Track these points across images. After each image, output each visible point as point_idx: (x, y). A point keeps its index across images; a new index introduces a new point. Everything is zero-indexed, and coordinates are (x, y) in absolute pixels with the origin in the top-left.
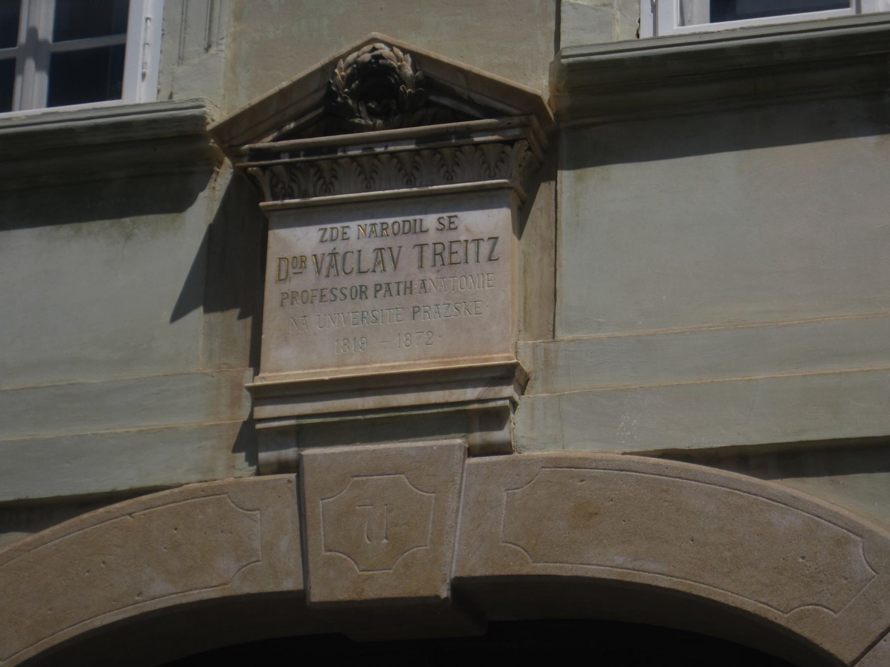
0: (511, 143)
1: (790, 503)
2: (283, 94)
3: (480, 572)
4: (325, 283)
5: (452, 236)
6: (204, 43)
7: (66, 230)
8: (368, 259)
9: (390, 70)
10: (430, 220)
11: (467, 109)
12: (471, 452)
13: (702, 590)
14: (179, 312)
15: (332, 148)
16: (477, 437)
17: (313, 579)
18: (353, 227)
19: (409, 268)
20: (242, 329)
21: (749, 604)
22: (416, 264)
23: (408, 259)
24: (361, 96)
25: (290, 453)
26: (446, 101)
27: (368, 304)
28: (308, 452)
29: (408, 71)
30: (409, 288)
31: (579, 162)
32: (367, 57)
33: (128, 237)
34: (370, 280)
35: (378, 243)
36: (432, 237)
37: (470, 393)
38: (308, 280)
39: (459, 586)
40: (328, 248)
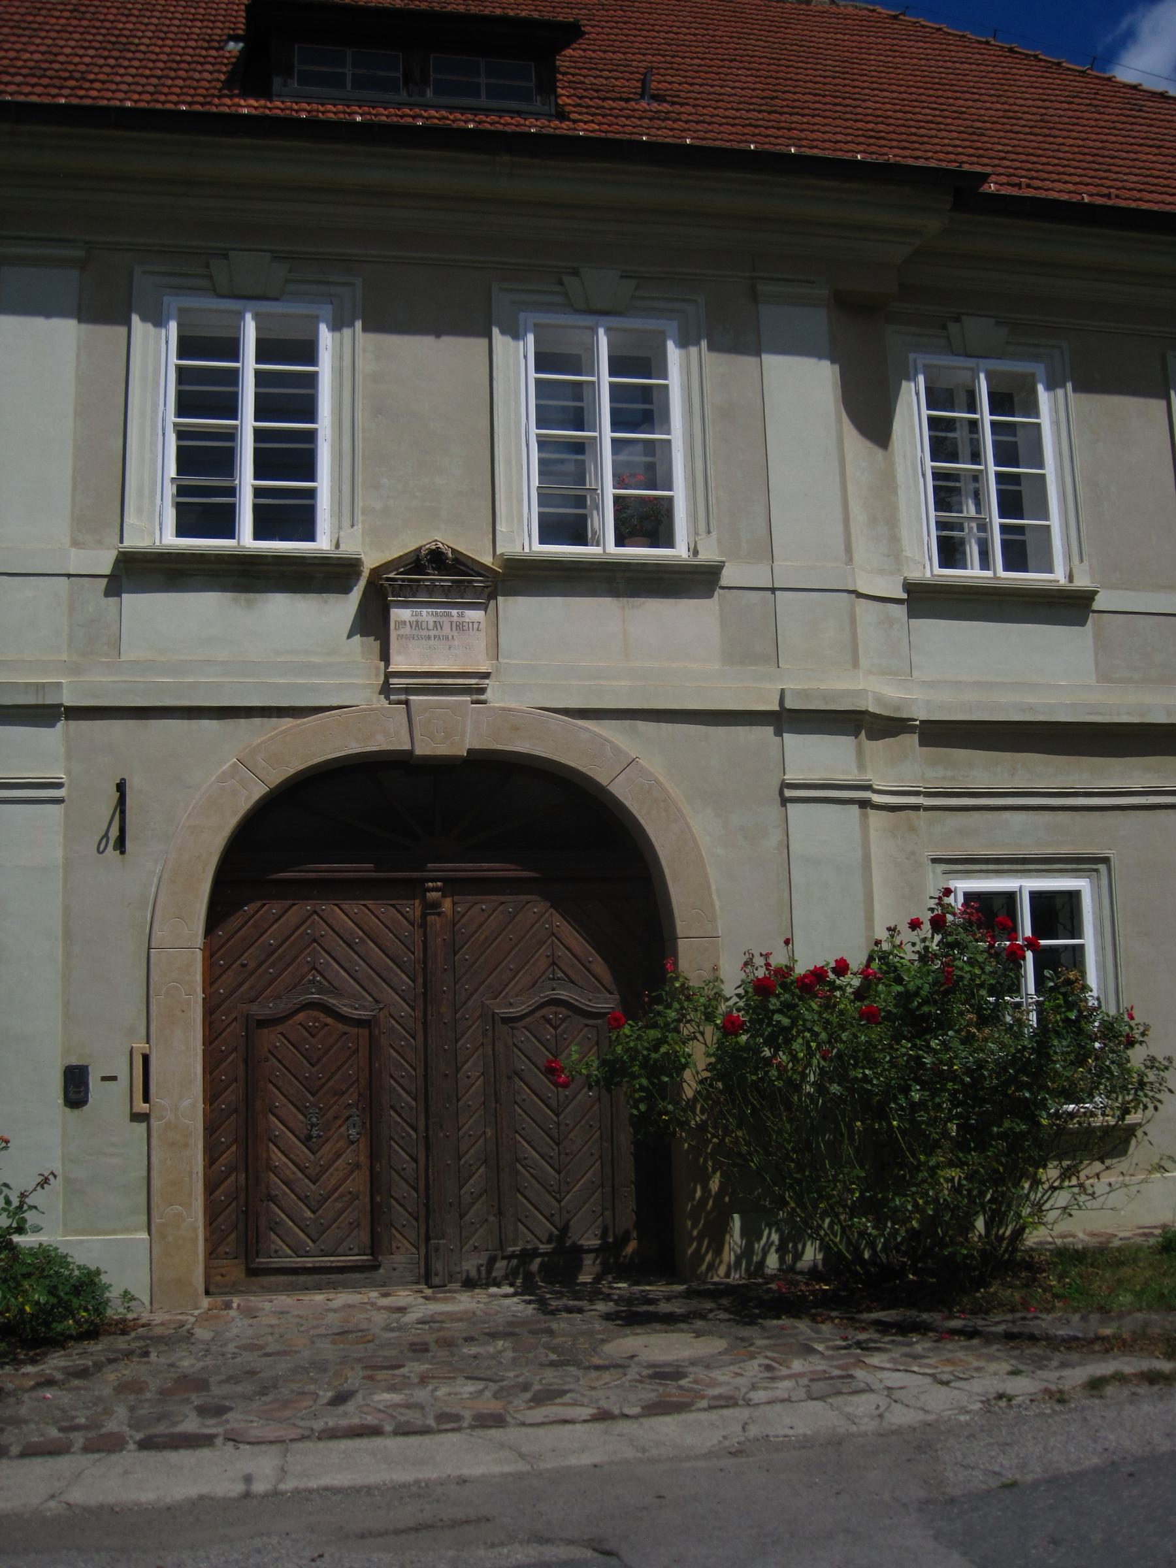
0: (487, 587)
1: (586, 729)
2: (400, 557)
3: (477, 747)
4: (414, 632)
5: (463, 619)
6: (350, 523)
7: (298, 596)
8: (431, 626)
9: (442, 553)
10: (454, 612)
11: (471, 572)
12: (473, 703)
13: (556, 758)
14: (350, 636)
15: (418, 580)
16: (475, 697)
17: (416, 745)
18: (424, 611)
19: (447, 630)
20: (374, 645)
21: (572, 764)
22: (939, 854)
23: (447, 626)
24: (429, 561)
25: (403, 697)
26: (462, 568)
27: (432, 642)
28: (411, 698)
29: (450, 555)
30: (447, 638)
31: (506, 594)
32: (434, 547)
33: (326, 602)
34: (432, 633)
35: (435, 619)
36: (455, 619)
37: (473, 681)
38: (407, 630)
39: (470, 751)
40: (414, 619)
